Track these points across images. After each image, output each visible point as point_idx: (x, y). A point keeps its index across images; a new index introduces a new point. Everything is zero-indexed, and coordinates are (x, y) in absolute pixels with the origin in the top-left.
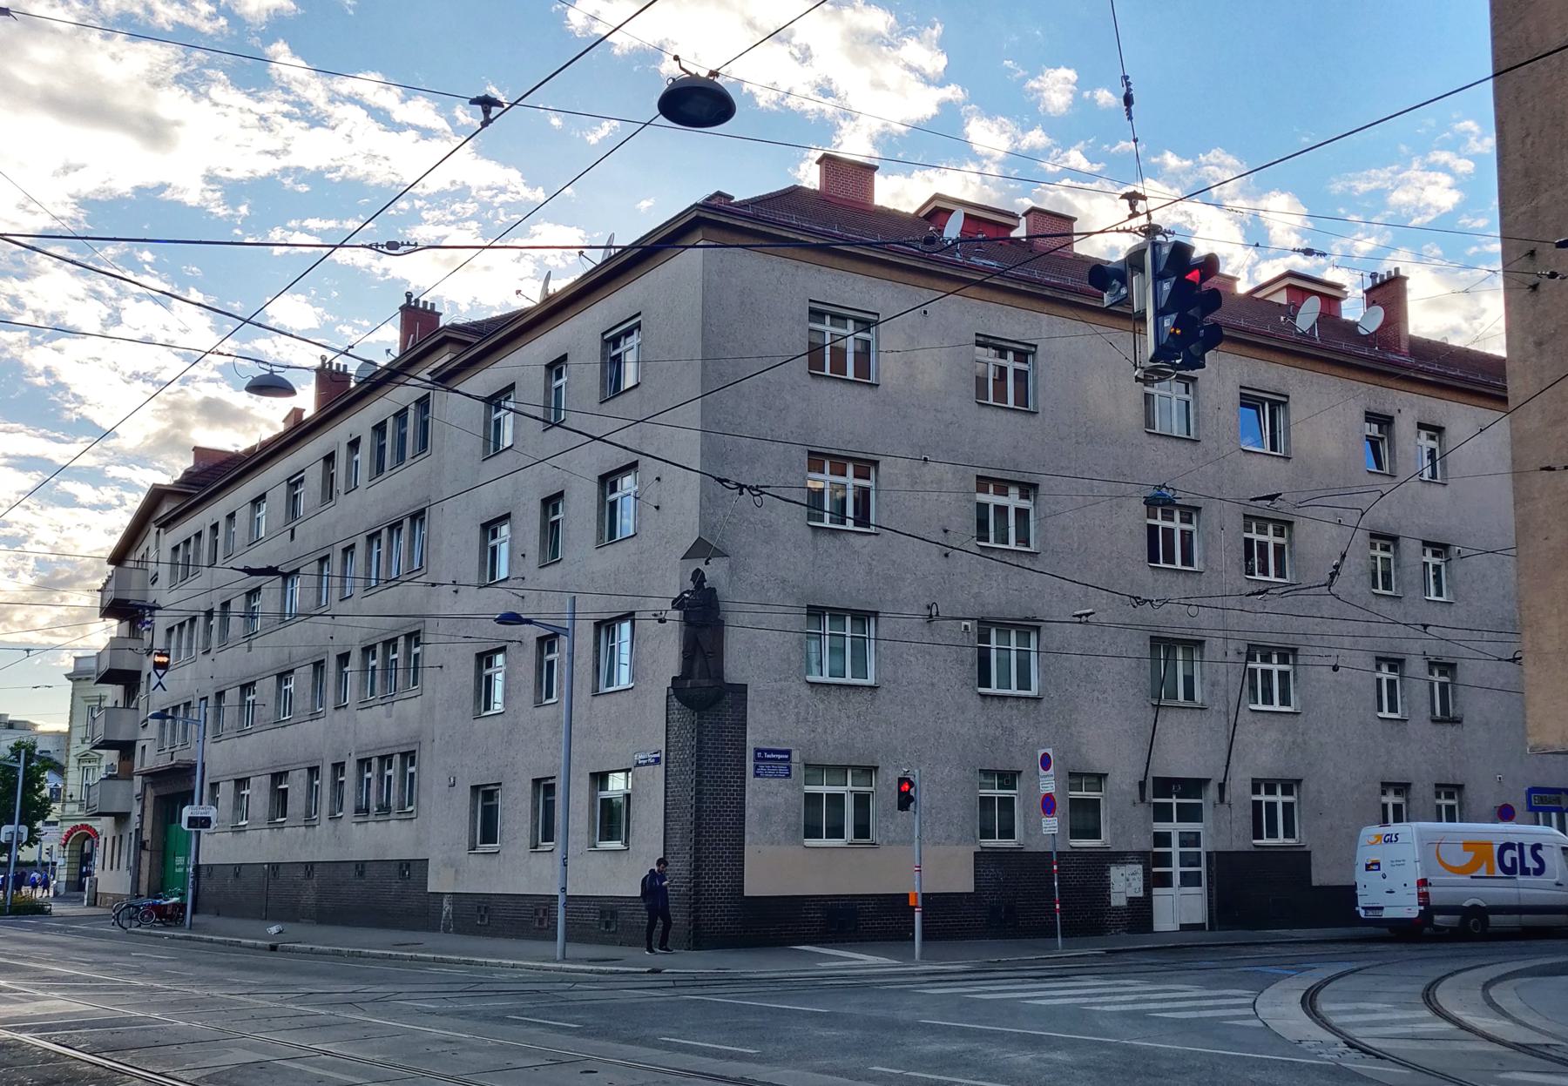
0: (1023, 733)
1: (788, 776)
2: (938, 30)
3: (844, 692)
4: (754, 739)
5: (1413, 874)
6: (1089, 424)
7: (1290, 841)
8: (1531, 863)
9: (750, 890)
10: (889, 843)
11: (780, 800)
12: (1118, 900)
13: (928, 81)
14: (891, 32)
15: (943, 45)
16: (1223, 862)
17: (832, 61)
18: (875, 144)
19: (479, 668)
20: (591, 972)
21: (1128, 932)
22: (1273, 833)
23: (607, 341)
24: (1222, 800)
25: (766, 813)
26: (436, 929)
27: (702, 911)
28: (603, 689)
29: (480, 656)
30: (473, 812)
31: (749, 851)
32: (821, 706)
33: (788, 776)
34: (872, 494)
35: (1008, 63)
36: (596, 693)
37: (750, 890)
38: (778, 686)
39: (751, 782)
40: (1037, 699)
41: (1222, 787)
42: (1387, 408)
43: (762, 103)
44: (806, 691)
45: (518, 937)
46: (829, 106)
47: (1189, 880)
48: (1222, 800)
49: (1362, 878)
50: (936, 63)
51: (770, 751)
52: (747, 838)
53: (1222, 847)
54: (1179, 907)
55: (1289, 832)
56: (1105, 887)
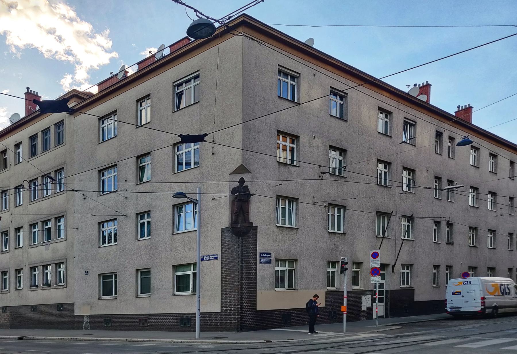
0: (340, 247)
1: (270, 263)
2: (108, 32)
3: (288, 230)
4: (260, 249)
5: (478, 295)
6: (362, 127)
7: (408, 286)
8: (507, 291)
9: (258, 309)
10: (301, 289)
11: (268, 273)
12: (364, 308)
13: (106, 51)
14: (91, 32)
15: (110, 37)
16: (391, 293)
17: (71, 42)
18: (88, 73)
19: (99, 228)
20: (236, 343)
21: (366, 319)
22: (404, 284)
23: (175, 86)
24: (393, 272)
25: (264, 278)
26: (81, 329)
27: (246, 316)
28: (176, 232)
29: (99, 223)
30: (99, 284)
31: (258, 292)
32: (281, 236)
33: (270, 263)
34: (295, 149)
35: (134, 45)
36: (174, 234)
37: (258, 309)
38: (267, 227)
39: (259, 266)
40: (344, 234)
41: (393, 267)
42: (441, 130)
43: (46, 56)
44: (276, 229)
45: (129, 330)
46: (71, 58)
47: (381, 300)
48: (393, 272)
49: (449, 297)
50: (109, 44)
51: (265, 254)
52: (258, 287)
53: (392, 288)
54: (380, 309)
55: (408, 284)
56: (360, 304)
